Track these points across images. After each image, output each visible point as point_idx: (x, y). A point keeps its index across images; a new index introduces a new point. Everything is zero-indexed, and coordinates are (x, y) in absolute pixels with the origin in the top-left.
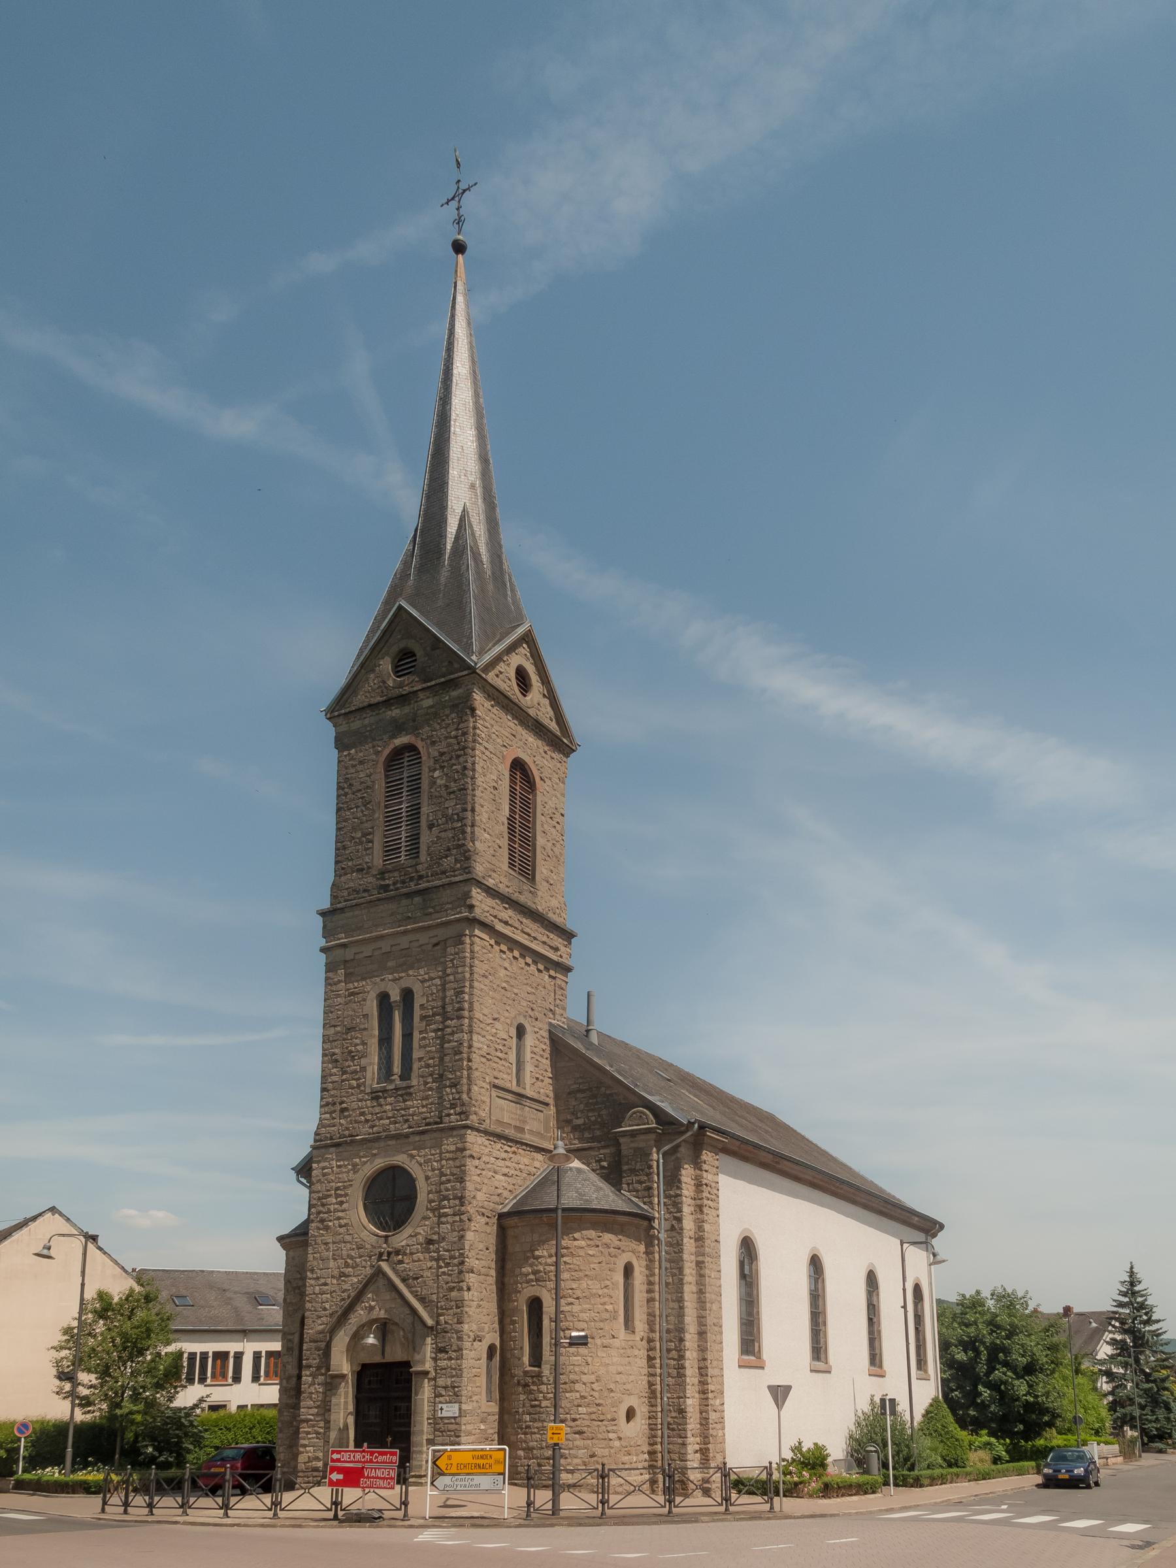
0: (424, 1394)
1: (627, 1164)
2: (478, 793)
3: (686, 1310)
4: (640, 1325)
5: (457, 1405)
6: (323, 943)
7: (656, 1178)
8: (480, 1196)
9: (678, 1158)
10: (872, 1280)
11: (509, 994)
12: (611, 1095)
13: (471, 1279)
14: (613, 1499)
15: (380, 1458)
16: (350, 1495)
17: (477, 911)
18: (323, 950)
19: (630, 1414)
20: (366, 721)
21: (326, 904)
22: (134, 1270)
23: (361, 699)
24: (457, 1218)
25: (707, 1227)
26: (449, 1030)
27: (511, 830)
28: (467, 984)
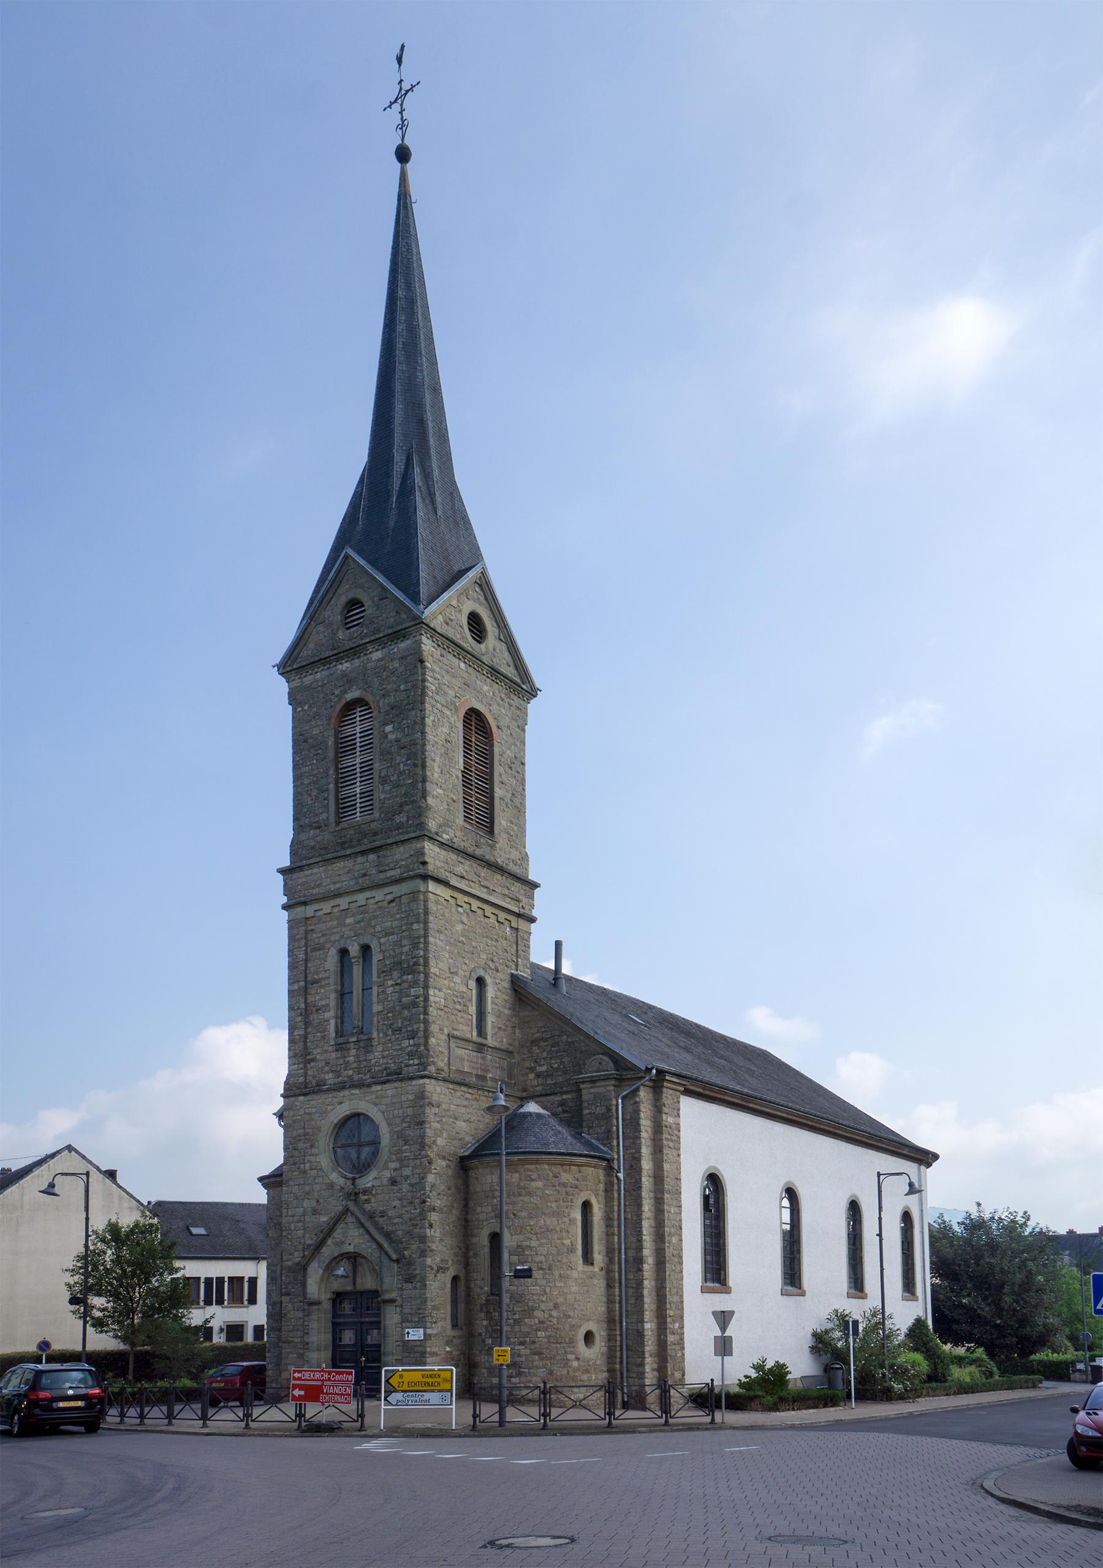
0: (391, 1318)
1: (587, 1108)
2: (428, 748)
3: (645, 1244)
4: (599, 1257)
5: (422, 1330)
6: (285, 900)
7: (615, 1121)
8: (440, 1141)
9: (636, 1103)
10: (854, 1209)
11: (467, 948)
12: (573, 1042)
13: (434, 1217)
14: (555, 1412)
15: (337, 1377)
16: (312, 1410)
17: (430, 867)
18: (285, 907)
19: (589, 1337)
20: (318, 676)
21: (286, 862)
22: (149, 1203)
23: (307, 653)
24: (418, 1162)
25: (666, 1166)
26: (405, 985)
27: (466, 782)
28: (422, 940)
